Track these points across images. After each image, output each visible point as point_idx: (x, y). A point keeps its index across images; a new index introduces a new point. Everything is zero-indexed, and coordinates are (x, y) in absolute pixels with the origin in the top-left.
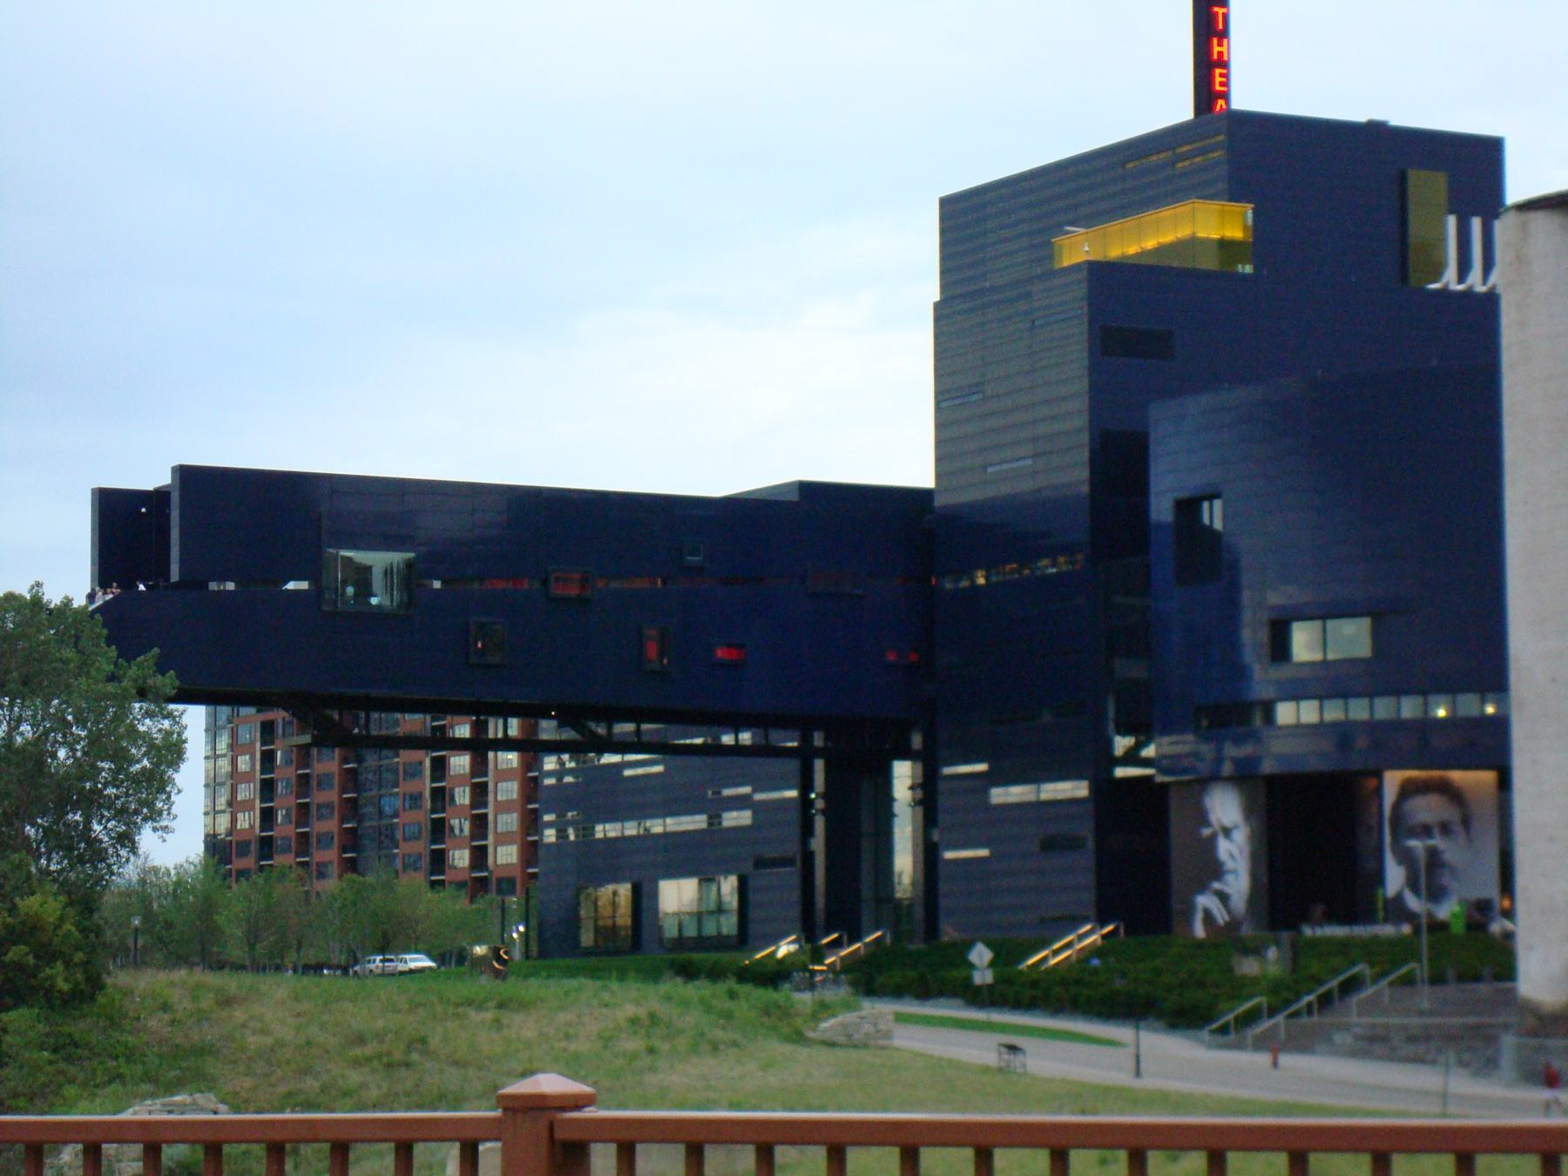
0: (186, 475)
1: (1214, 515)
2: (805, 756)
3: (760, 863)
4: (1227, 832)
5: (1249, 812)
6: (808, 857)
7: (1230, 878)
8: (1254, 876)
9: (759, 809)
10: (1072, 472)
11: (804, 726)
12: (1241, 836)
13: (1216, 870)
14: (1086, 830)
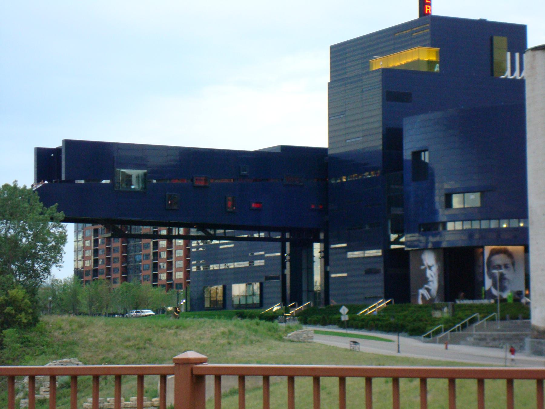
0: (68, 143)
1: (426, 157)
2: (283, 241)
3: (267, 278)
4: (430, 267)
5: (437, 261)
6: (284, 276)
7: (431, 283)
8: (439, 282)
9: (267, 260)
10: (376, 142)
11: (283, 231)
12: (435, 269)
13: (425, 281)
14: (381, 267)
